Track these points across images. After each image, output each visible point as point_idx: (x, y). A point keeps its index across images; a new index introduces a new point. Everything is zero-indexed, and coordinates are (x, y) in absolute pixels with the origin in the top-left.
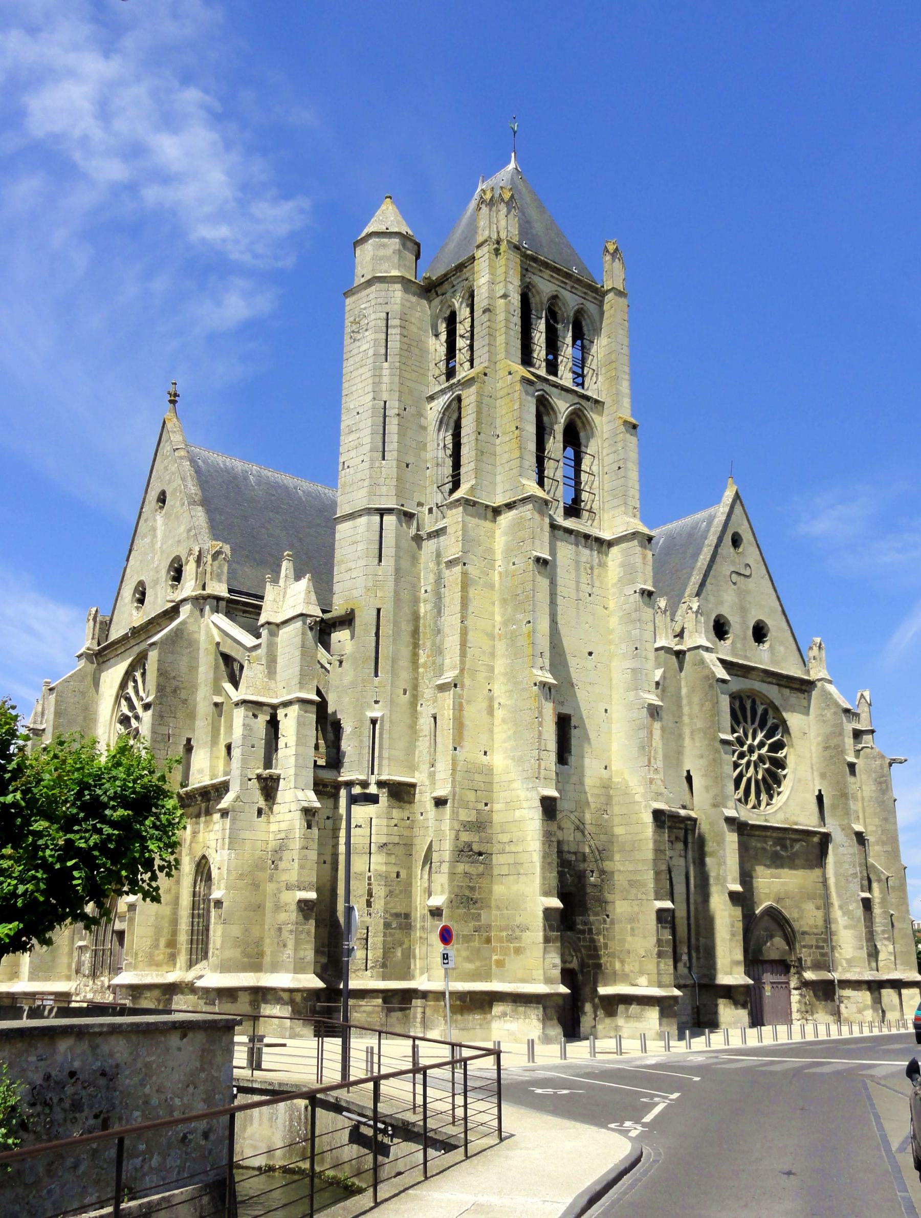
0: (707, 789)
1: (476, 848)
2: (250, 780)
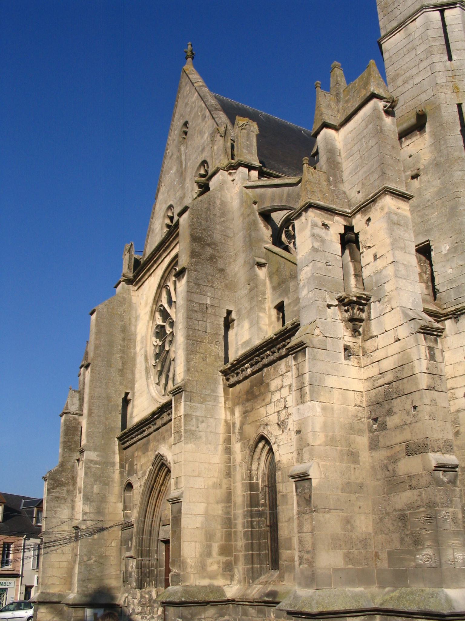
2: (329, 306)
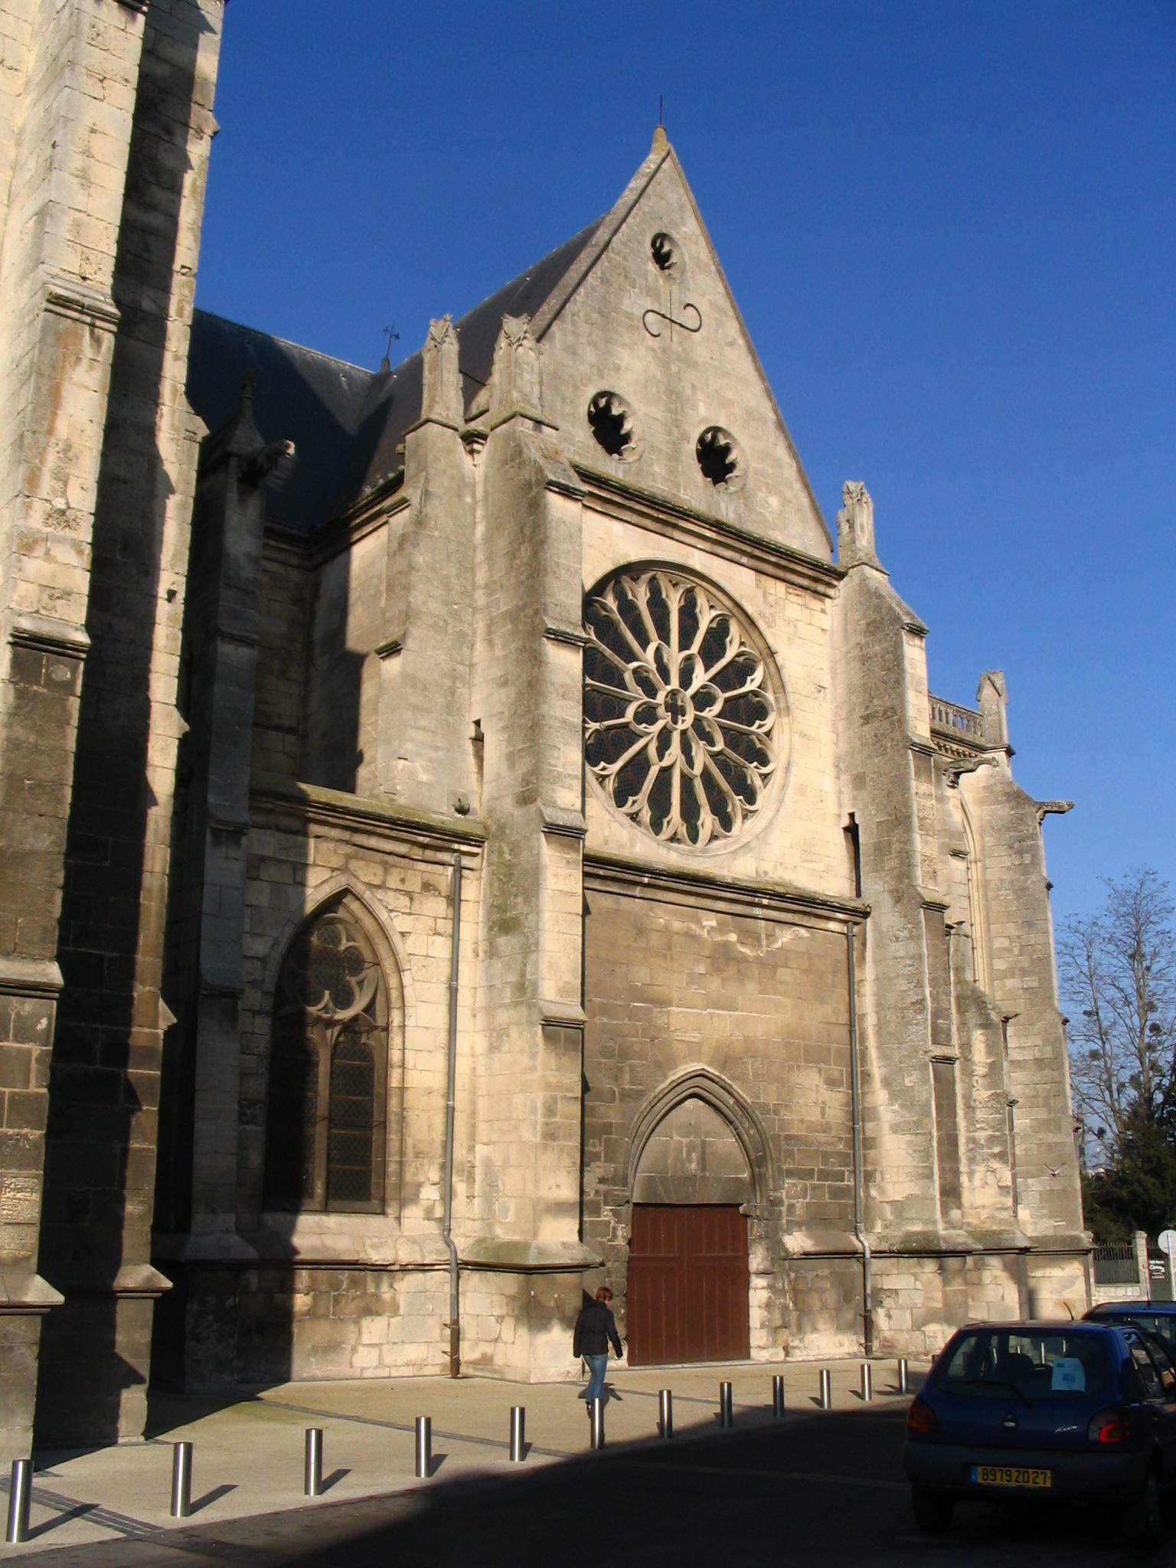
0: (511, 759)
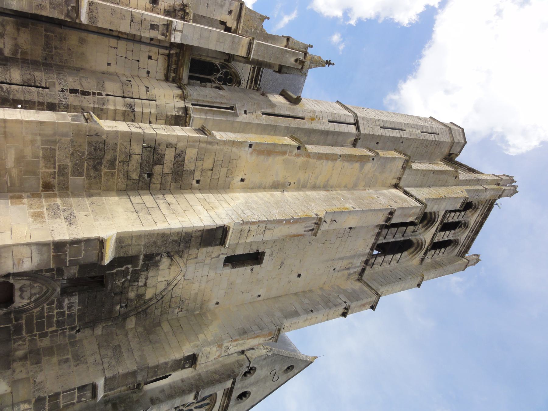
1: (158, 169)
